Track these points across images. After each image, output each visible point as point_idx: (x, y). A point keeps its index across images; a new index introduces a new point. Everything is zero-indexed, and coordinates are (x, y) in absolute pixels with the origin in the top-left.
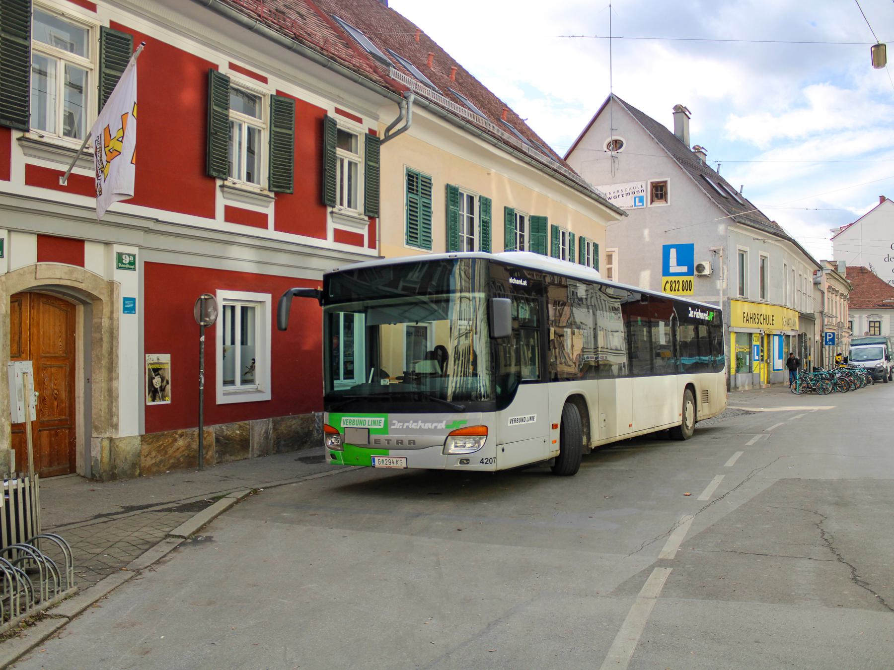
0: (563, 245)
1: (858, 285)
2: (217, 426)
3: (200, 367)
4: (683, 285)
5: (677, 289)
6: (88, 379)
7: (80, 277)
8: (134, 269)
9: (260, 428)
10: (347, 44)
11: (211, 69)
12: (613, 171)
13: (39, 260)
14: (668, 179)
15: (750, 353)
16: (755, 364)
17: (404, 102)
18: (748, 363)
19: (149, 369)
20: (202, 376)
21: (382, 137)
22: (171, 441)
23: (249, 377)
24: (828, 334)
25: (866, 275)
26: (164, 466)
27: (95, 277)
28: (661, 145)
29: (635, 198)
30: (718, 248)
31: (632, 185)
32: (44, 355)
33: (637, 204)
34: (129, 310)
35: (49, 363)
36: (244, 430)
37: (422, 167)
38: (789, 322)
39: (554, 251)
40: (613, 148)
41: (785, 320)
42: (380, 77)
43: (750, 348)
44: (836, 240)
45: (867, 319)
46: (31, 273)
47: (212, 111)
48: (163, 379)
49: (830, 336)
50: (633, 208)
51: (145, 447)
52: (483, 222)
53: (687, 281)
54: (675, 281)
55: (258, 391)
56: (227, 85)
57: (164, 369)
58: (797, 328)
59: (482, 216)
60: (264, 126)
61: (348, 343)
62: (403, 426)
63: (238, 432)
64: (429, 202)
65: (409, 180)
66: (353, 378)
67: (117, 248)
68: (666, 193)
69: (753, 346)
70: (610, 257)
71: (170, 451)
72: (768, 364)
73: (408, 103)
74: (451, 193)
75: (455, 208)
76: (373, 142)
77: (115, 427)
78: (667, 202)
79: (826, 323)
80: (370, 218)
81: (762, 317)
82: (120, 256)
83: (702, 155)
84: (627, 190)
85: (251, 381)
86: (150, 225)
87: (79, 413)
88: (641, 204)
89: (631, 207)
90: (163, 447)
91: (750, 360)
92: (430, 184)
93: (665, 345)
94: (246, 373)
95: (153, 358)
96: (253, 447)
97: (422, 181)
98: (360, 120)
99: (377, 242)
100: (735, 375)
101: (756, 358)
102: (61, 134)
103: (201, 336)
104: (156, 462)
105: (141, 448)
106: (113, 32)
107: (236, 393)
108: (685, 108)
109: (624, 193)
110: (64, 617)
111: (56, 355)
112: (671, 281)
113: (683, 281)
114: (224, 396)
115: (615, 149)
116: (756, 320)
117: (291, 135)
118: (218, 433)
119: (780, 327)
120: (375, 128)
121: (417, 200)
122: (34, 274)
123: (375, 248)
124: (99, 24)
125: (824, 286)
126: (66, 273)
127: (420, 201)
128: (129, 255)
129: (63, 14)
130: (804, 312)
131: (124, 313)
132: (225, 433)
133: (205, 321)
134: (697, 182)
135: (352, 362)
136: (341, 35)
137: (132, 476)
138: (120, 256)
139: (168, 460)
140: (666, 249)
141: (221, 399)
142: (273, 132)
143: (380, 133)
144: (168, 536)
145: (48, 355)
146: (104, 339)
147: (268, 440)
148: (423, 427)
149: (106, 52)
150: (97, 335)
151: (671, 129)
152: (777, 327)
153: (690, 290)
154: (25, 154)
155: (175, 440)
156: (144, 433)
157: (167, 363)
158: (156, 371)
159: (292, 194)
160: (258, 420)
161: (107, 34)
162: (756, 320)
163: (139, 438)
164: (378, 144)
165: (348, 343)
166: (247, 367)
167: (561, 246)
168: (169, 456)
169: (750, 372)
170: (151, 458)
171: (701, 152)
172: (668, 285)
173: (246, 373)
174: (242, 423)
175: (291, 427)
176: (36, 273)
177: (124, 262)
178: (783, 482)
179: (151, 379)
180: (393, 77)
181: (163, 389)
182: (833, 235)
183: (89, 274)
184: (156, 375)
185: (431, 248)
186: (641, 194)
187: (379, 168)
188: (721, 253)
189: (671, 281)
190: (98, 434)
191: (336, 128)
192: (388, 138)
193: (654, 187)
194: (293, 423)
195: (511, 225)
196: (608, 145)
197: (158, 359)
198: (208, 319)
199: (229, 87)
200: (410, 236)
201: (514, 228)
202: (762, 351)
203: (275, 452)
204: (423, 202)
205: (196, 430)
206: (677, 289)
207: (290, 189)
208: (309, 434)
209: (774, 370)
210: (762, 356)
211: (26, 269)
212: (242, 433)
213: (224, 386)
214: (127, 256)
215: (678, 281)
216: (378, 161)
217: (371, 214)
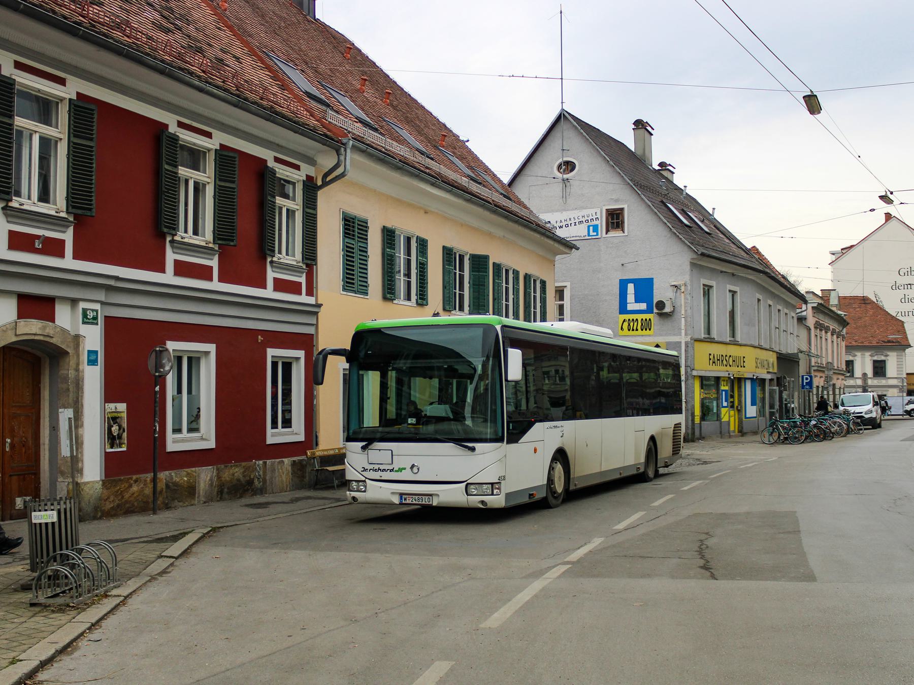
0: (506, 284)
1: (860, 318)
2: (167, 473)
3: (155, 415)
4: (642, 324)
5: (635, 328)
6: (54, 427)
7: (51, 333)
8: (97, 324)
9: (205, 476)
10: (282, 85)
11: (163, 130)
12: (564, 197)
13: (19, 318)
14: (625, 206)
15: (717, 399)
16: (724, 411)
17: (342, 149)
18: (715, 411)
19: (108, 418)
20: (157, 425)
21: (319, 183)
22: (127, 486)
23: (194, 425)
24: (805, 377)
25: (869, 306)
26: (121, 510)
27: (63, 330)
28: (617, 169)
29: (589, 227)
30: (680, 283)
31: (585, 212)
32: (14, 404)
33: (591, 233)
34: (92, 362)
35: (18, 412)
36: (191, 477)
37: (358, 209)
38: (760, 363)
39: (496, 291)
40: (564, 171)
41: (759, 361)
42: (317, 121)
43: (718, 393)
44: (836, 265)
45: (870, 358)
46: (12, 329)
47: (164, 170)
48: (120, 427)
49: (807, 379)
50: (587, 238)
51: (105, 492)
52: (420, 264)
53: (646, 320)
54: (633, 320)
55: (202, 439)
56: (177, 144)
57: (121, 417)
58: (775, 371)
59: (419, 258)
60: (208, 180)
61: (285, 391)
63: (186, 479)
64: (365, 246)
65: (345, 225)
66: (291, 427)
67: (82, 305)
68: (623, 222)
69: (720, 391)
70: (560, 293)
71: (127, 496)
72: (739, 411)
73: (345, 150)
74: (388, 235)
75: (392, 251)
76: (311, 188)
77: (81, 471)
78: (624, 232)
79: (813, 364)
80: (307, 265)
81: (731, 359)
82: (85, 311)
83: (669, 172)
84: (580, 217)
85: (197, 430)
86: (112, 283)
87: (44, 459)
88: (595, 234)
89: (584, 236)
90: (120, 492)
91: (718, 406)
92: (366, 227)
94: (192, 422)
95: (111, 406)
96: (199, 493)
97: (358, 225)
98: (297, 168)
99: (315, 289)
100: (700, 423)
101: (725, 404)
102: (36, 201)
103: (156, 386)
104: (113, 506)
105: (102, 492)
106: (80, 104)
107: (183, 441)
108: (647, 122)
109: (577, 221)
110: (120, 596)
111: (25, 404)
112: (629, 320)
113: (642, 319)
114: (175, 443)
115: (567, 172)
116: (725, 362)
117: (234, 188)
118: (168, 479)
119: (753, 369)
120: (313, 175)
121: (353, 244)
122: (14, 330)
123: (312, 296)
124: (68, 96)
125: (811, 322)
126: (40, 329)
127: (357, 245)
128: (93, 310)
129: (39, 91)
130: (784, 352)
131: (88, 365)
132: (174, 480)
133: (160, 372)
134: (656, 210)
135: (290, 411)
136: (276, 75)
137: (95, 518)
138: (85, 311)
139: (125, 505)
140: (623, 284)
141: (171, 447)
142: (217, 186)
143: (316, 179)
144: (161, 557)
145: (17, 404)
146: (70, 389)
147: (213, 488)
149: (74, 127)
150: (64, 386)
151: (631, 146)
152: (750, 370)
153: (650, 330)
154: (8, 222)
155: (131, 486)
156: (104, 478)
157: (124, 412)
158: (115, 419)
159: (235, 246)
160: (204, 468)
161: (75, 106)
162: (725, 362)
163: (101, 482)
164: (315, 191)
165: (285, 391)
166: (192, 416)
167: (504, 285)
168: (126, 501)
169: (717, 420)
170: (110, 502)
171: (668, 170)
172: (626, 324)
173: (192, 422)
174: (189, 470)
175: (233, 475)
176: (16, 329)
177: (89, 317)
178: (696, 515)
179: (110, 427)
180: (329, 120)
181: (120, 437)
182: (834, 258)
183: (58, 329)
184: (114, 424)
185: (368, 293)
186: (595, 222)
187: (316, 215)
188: (683, 288)
189: (629, 320)
190: (64, 479)
191: (275, 177)
192: (325, 184)
193: (609, 214)
194: (235, 472)
195: (449, 265)
196: (559, 167)
197: (116, 408)
198: (162, 370)
199: (178, 145)
200: (347, 282)
201: (453, 268)
202: (732, 397)
203: (218, 499)
204: (360, 246)
205: (150, 476)
206: (635, 328)
207: (233, 241)
208: (250, 482)
209: (746, 418)
210: (733, 402)
211: (8, 326)
212: (190, 480)
213: (173, 434)
214: (91, 312)
215: (637, 320)
216: (315, 209)
217: (309, 262)
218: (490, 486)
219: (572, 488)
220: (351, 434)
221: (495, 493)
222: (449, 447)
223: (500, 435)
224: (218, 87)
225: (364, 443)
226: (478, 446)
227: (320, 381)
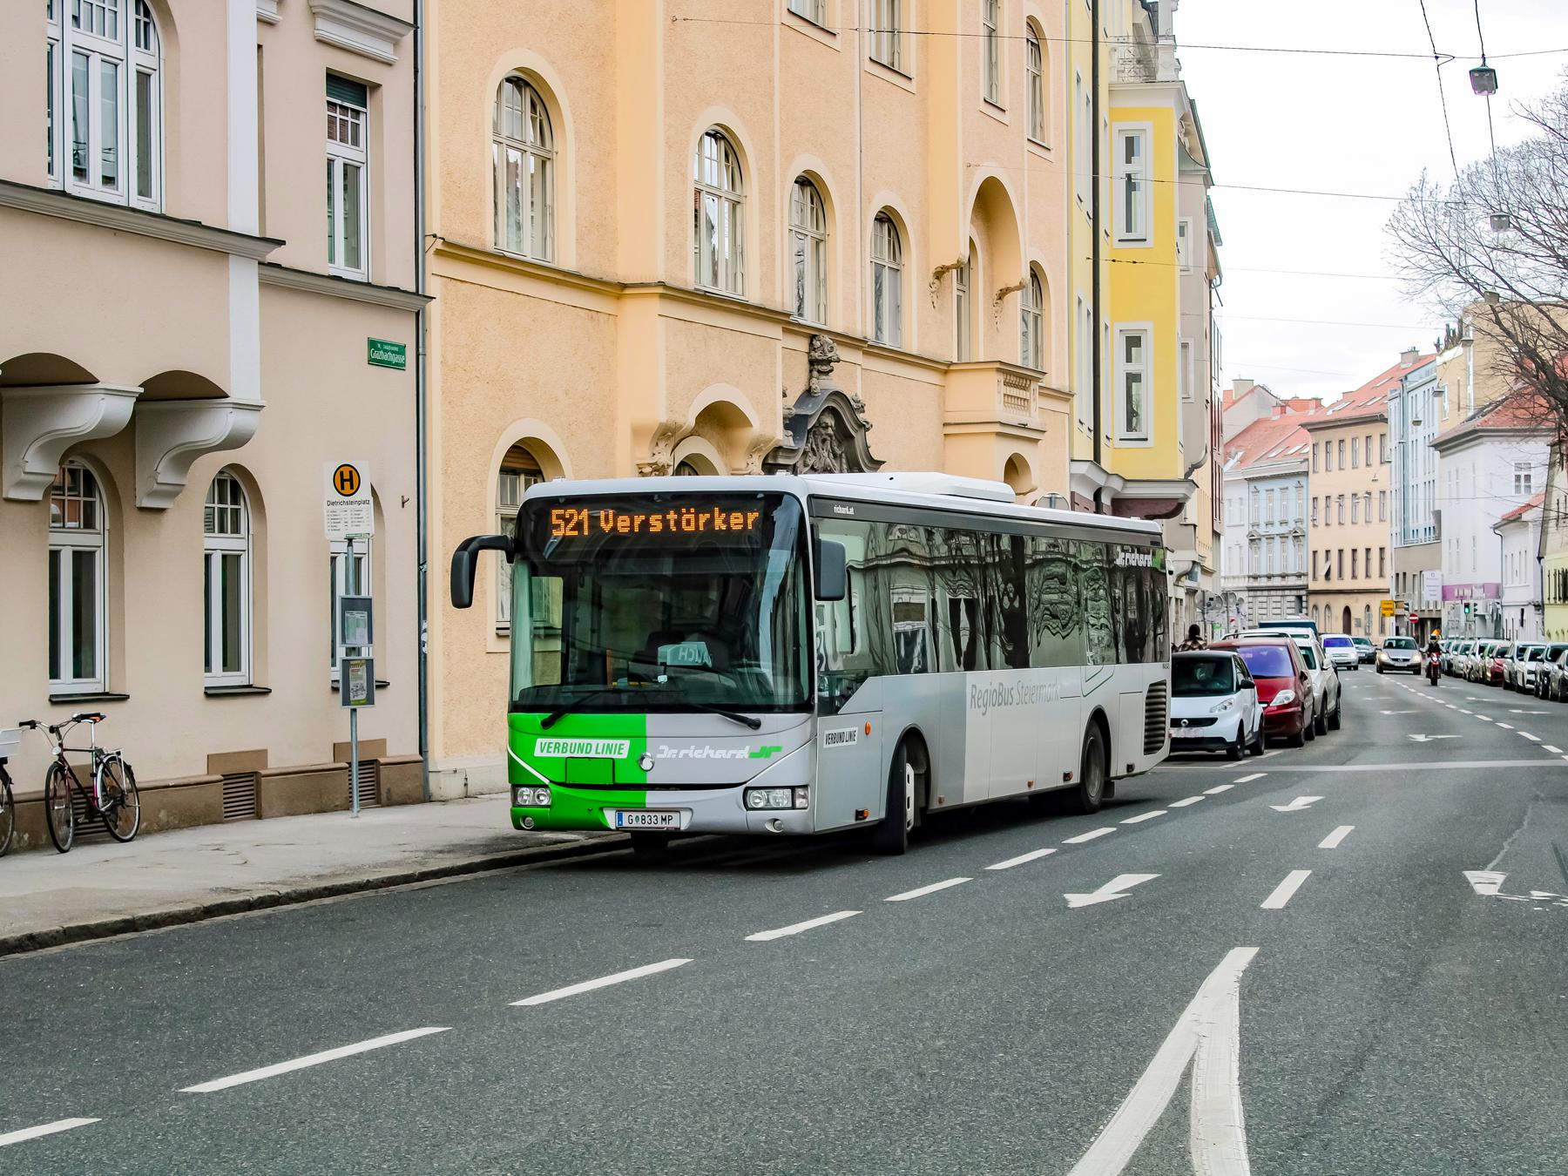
62: (678, 754)
93: (563, 641)
148: (712, 756)
218: (788, 792)
219: (935, 805)
220: (516, 698)
221: (797, 806)
222: (711, 722)
223: (806, 696)
224: (903, 593)
225: (546, 715)
226: (765, 718)
227: (466, 600)
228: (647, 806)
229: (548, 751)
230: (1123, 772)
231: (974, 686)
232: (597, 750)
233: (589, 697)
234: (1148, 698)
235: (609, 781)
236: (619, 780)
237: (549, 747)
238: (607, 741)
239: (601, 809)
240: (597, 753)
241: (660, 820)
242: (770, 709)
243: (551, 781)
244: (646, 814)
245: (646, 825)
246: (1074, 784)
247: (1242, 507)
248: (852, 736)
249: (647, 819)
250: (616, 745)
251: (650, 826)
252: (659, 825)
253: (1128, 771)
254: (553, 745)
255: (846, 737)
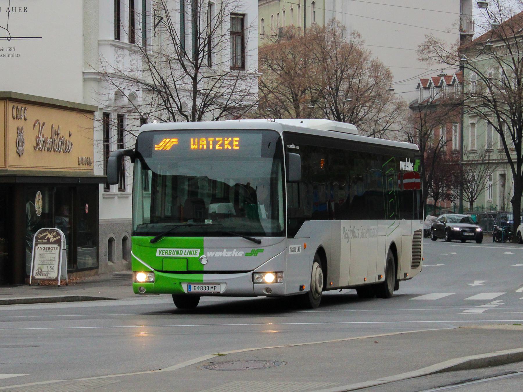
220: (135, 229)
228: (204, 281)
229: (162, 254)
230: (402, 277)
231: (344, 228)
232: (185, 253)
233: (176, 228)
234: (414, 238)
235: (185, 269)
236: (191, 269)
237: (163, 252)
238: (189, 250)
239: (180, 283)
240: (185, 254)
241: (210, 288)
242: (264, 234)
243: (154, 270)
244: (203, 286)
245: (203, 291)
246: (382, 282)
247: (456, 134)
248: (299, 248)
249: (204, 288)
250: (194, 251)
251: (205, 291)
252: (210, 291)
253: (405, 277)
254: (165, 251)
255: (297, 249)
